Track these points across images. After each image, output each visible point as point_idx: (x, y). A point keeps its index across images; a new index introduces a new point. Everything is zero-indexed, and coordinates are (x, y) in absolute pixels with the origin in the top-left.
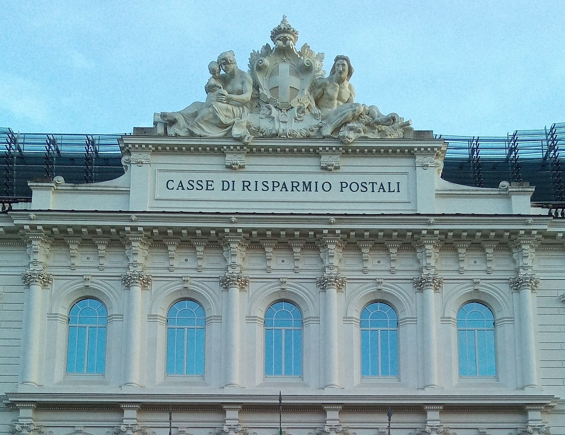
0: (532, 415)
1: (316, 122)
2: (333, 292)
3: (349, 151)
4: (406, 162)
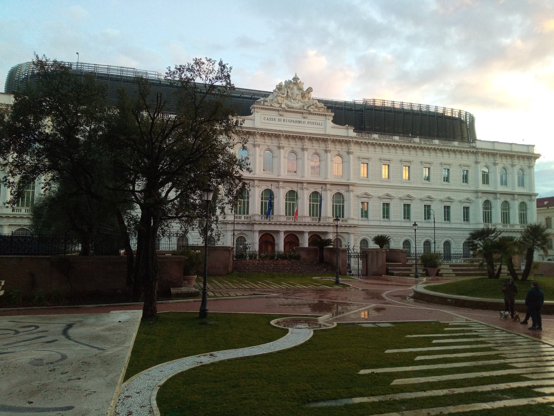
0: (350, 187)
1: (302, 104)
2: (282, 150)
3: (310, 113)
4: (324, 117)
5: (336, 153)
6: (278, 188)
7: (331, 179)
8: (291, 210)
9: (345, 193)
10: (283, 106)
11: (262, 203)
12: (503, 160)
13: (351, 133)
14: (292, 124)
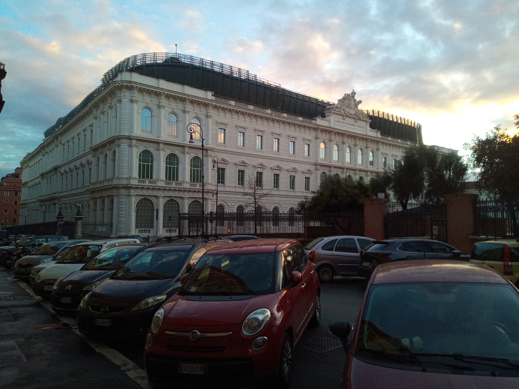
3: (360, 119)
5: (144, 105)
6: (184, 153)
7: (164, 137)
8: (172, 174)
9: (155, 152)
12: (306, 132)
13: (210, 95)
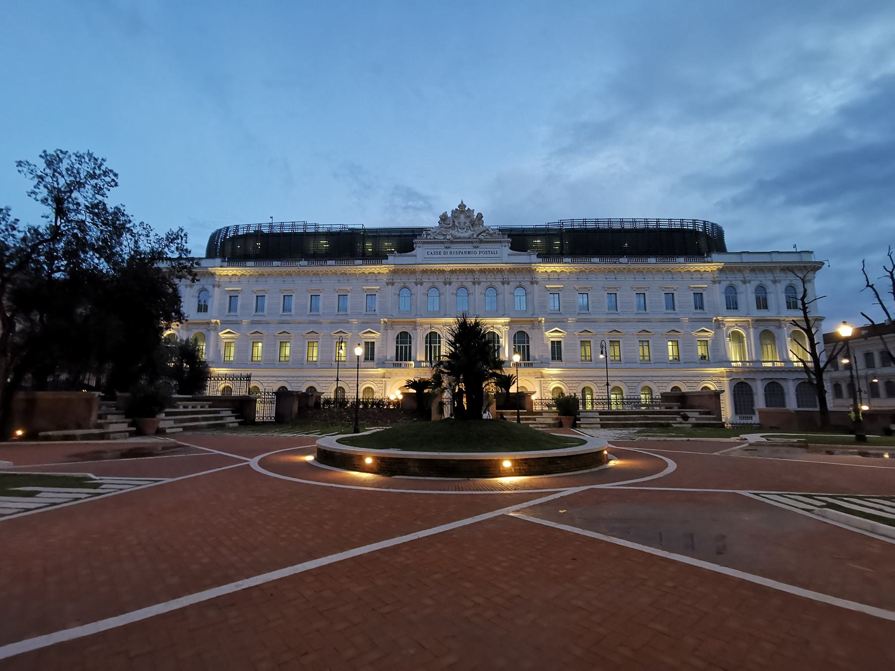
3: (481, 242)
10: (448, 237)
11: (397, 347)
14: (461, 255)
